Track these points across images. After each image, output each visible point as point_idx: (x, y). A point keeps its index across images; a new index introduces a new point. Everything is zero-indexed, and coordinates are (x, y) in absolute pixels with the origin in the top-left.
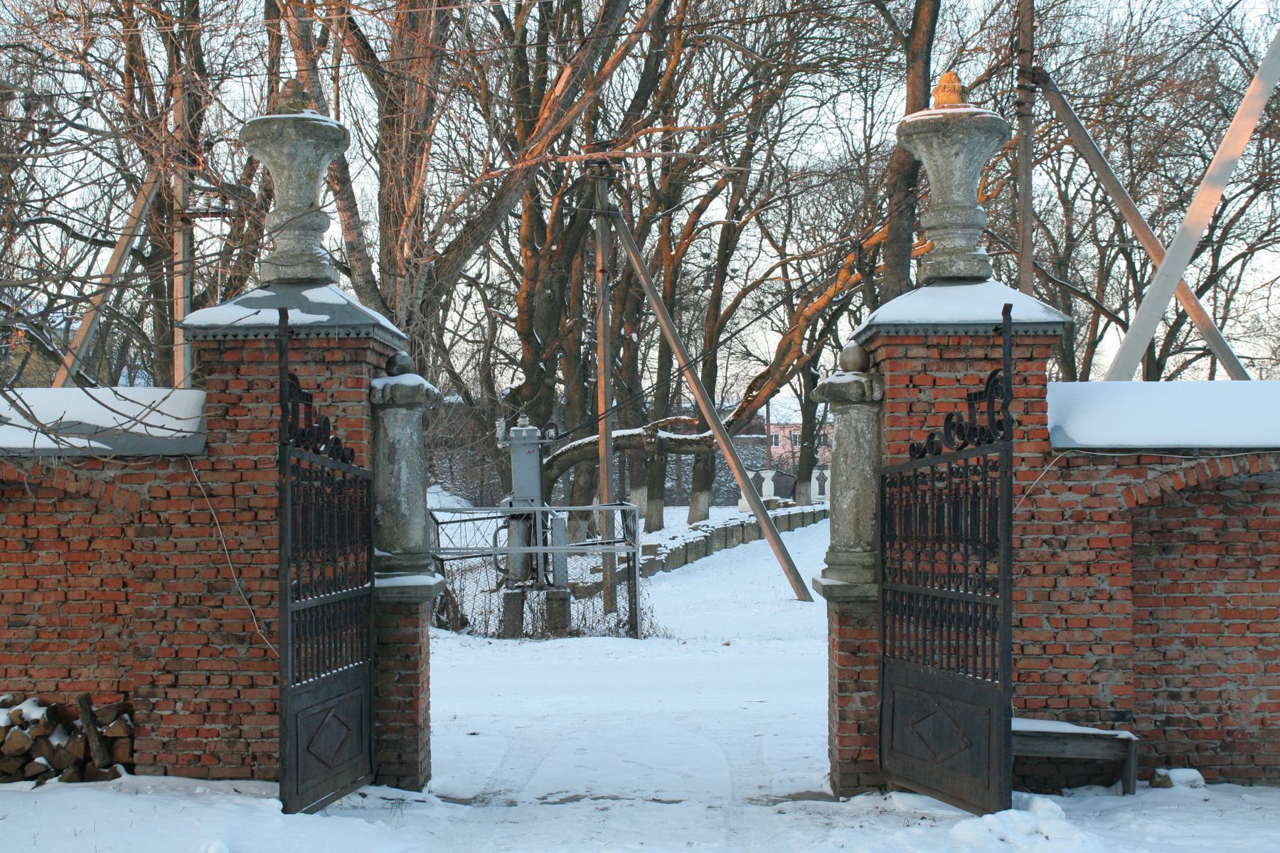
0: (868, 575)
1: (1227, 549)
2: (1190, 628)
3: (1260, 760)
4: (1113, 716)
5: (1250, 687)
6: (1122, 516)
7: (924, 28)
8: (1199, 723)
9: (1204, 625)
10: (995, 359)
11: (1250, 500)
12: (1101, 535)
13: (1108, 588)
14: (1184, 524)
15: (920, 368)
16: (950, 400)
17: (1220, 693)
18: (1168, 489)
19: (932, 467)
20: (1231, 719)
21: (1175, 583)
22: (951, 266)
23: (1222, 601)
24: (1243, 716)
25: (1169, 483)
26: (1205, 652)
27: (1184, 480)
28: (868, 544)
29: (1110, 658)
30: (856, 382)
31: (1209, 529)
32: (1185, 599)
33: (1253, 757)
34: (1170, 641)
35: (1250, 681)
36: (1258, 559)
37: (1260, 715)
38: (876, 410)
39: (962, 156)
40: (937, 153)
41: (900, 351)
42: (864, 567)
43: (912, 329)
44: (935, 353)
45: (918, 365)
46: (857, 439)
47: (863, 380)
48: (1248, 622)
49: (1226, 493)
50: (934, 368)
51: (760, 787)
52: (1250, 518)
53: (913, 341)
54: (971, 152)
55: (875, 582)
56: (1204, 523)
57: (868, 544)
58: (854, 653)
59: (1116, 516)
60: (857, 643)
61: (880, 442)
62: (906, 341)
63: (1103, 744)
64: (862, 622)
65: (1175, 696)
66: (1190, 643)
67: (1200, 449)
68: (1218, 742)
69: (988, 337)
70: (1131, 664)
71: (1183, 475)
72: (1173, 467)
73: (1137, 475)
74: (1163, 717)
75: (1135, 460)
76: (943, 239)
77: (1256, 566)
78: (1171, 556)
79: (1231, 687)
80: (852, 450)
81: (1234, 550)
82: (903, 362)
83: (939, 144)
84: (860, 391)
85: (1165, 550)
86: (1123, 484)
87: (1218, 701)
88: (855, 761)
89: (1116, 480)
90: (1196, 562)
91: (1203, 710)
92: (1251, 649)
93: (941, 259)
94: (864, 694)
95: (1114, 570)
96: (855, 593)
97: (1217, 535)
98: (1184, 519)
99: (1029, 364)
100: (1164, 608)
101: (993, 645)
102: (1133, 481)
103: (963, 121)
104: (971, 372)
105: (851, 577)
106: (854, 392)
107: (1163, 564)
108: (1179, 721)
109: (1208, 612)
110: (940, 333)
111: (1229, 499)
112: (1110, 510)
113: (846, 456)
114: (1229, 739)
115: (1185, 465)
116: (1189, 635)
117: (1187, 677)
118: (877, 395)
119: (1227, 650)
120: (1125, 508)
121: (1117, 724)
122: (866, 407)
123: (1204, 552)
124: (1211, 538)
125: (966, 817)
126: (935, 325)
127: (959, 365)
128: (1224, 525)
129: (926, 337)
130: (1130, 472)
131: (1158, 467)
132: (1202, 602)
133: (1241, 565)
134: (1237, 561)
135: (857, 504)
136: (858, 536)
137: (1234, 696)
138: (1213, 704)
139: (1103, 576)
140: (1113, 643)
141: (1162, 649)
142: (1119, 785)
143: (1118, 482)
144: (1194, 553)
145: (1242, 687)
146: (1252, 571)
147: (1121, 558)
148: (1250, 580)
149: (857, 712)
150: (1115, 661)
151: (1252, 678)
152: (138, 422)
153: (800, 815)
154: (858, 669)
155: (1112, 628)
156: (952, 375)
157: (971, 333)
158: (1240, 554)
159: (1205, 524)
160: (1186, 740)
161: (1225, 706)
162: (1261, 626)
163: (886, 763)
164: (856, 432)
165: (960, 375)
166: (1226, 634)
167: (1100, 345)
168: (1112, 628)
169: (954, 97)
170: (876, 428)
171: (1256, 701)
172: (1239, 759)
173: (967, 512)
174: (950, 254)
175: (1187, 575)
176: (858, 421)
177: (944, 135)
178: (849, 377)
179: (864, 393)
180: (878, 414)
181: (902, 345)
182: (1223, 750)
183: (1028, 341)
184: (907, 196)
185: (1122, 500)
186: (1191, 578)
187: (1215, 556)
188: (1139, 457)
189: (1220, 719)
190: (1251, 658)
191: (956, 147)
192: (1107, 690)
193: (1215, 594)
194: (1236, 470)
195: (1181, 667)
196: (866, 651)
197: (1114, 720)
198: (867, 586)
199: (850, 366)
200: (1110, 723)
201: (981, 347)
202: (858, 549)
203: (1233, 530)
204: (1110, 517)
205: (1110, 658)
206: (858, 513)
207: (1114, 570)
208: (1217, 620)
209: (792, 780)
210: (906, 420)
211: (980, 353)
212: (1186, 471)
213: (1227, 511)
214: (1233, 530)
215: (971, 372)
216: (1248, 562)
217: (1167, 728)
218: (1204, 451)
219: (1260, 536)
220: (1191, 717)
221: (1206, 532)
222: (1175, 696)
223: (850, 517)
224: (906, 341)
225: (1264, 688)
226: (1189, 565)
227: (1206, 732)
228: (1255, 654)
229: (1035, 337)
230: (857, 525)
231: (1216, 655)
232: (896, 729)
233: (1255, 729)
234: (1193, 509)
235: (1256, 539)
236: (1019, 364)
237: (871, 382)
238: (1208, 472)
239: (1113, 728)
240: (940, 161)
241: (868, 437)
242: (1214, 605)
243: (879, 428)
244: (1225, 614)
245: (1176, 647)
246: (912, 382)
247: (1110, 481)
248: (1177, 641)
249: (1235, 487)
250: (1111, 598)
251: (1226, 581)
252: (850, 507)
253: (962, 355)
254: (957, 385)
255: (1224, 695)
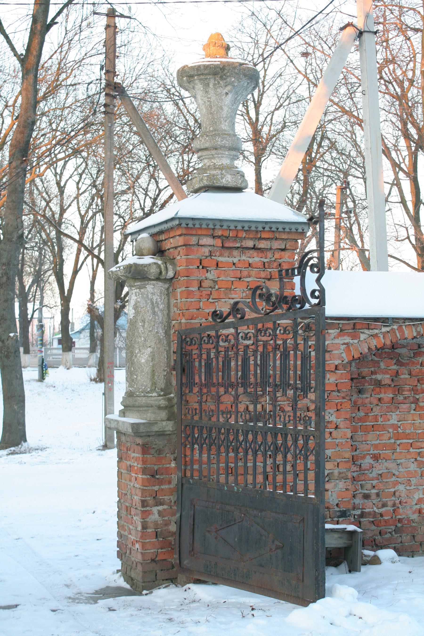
0: (164, 414)
1: (399, 390)
2: (376, 447)
3: (419, 538)
4: (338, 514)
5: (413, 487)
6: (344, 367)
7: (35, 53)
8: (381, 515)
9: (385, 445)
10: (260, 249)
11: (412, 355)
12: (331, 381)
13: (335, 420)
14: (372, 373)
15: (207, 254)
16: (229, 279)
17: (394, 493)
18: (373, 348)
19: (217, 332)
20: (401, 510)
21: (367, 415)
22: (222, 178)
23: (395, 427)
24: (408, 508)
25: (374, 343)
26: (386, 464)
27: (383, 341)
28: (162, 390)
29: (336, 472)
30: (155, 263)
31: (388, 376)
32: (373, 426)
33: (414, 536)
34: (364, 457)
35: (413, 483)
36: (417, 397)
37: (418, 507)
38: (166, 286)
39: (230, 96)
40: (211, 92)
41: (193, 240)
42: (160, 408)
43: (197, 223)
44: (218, 242)
45: (206, 251)
46: (153, 308)
47: (160, 262)
48: (411, 441)
49: (398, 351)
50: (218, 254)
51: (67, 586)
52: (412, 368)
53: (204, 232)
54: (237, 93)
55: (168, 419)
56: (385, 372)
57: (162, 390)
58: (153, 476)
59: (340, 367)
60: (156, 467)
61: (169, 311)
62: (199, 232)
63: (336, 535)
64: (159, 451)
65: (366, 497)
66: (376, 457)
67: (393, 318)
68: (393, 528)
69: (257, 232)
70: (349, 475)
71: (382, 337)
72: (376, 331)
73: (354, 337)
74: (358, 512)
75: (352, 326)
76: (214, 158)
77: (416, 401)
78: (365, 396)
79: (401, 487)
80: (149, 316)
81: (403, 391)
82: (195, 248)
83: (215, 85)
84: (158, 270)
85: (360, 392)
86: (344, 344)
87: (393, 498)
88: (153, 560)
89: (339, 341)
90: (380, 400)
91: (384, 505)
92: (413, 460)
93: (215, 172)
94: (160, 508)
95: (339, 407)
96: (155, 428)
97: (392, 380)
98: (373, 369)
99: (283, 253)
100: (359, 433)
101: (255, 465)
102: (351, 341)
103: (235, 68)
104: (243, 258)
105: (150, 416)
106: (154, 270)
107: (359, 402)
108: (369, 513)
109: (387, 436)
110: (225, 227)
111: (399, 355)
112: (337, 362)
113: (143, 321)
114: (399, 525)
115: (384, 330)
116: (376, 452)
117: (374, 482)
118: (171, 274)
119: (399, 461)
120: (346, 361)
121: (341, 519)
122: (160, 284)
123: (385, 393)
124: (388, 382)
125: (297, 608)
126: (221, 220)
127: (235, 253)
128: (397, 373)
129: (214, 229)
130: (349, 335)
131: (366, 331)
132: (383, 428)
133: (407, 401)
134: (405, 398)
135: (153, 359)
136: (154, 384)
137: (403, 495)
138: (390, 501)
139: (332, 411)
140: (339, 460)
141: (358, 463)
142: (344, 566)
143: (342, 342)
144: (378, 394)
145: (408, 488)
146: (413, 406)
147: (344, 398)
148: (412, 412)
149: (156, 523)
150: (340, 473)
151: (414, 481)
152: (182, 99)
153: (131, 611)
154: (156, 488)
155: (337, 449)
156: (230, 260)
157: (246, 228)
158: (406, 393)
159: (386, 373)
160: (374, 527)
161: (397, 502)
162: (419, 444)
163: (185, 562)
164: (152, 303)
165: (235, 260)
166: (398, 450)
167: (79, 273)
168: (337, 449)
169: (222, 51)
170: (166, 300)
171: (416, 496)
172: (406, 538)
173: (256, 365)
174: (221, 169)
175: (374, 409)
176: (153, 294)
177: (221, 78)
178: (148, 260)
179: (161, 273)
180: (168, 289)
181: (195, 235)
182: (396, 533)
183: (284, 236)
184: (22, 163)
185: (344, 355)
186: (376, 411)
187: (391, 396)
188: (354, 324)
189: (394, 511)
190: (413, 467)
191: (229, 88)
192: (335, 495)
193: (391, 422)
194: (415, 334)
195: (371, 475)
196: (162, 474)
197: (339, 517)
198: (164, 423)
199: (145, 252)
200: (336, 519)
201: (251, 239)
202: (155, 394)
203: (402, 376)
204: (336, 368)
205: (336, 472)
206: (153, 366)
207: (339, 407)
208: (392, 441)
209: (86, 577)
210: (197, 293)
211: (250, 244)
212: (384, 334)
213: (399, 363)
214: (402, 376)
215: (243, 258)
216: (411, 399)
217: (362, 520)
218: (395, 320)
219: (418, 381)
220: (377, 511)
221: (385, 378)
222: (366, 497)
223: (147, 369)
224: (199, 232)
225: (420, 488)
226: (375, 402)
227: (386, 521)
228: (416, 463)
229: (288, 233)
230: (153, 375)
231: (392, 465)
232: (197, 534)
233: (415, 517)
234: (378, 362)
235: (416, 383)
236: (276, 253)
237: (166, 263)
238: (398, 335)
239: (338, 523)
240: (213, 98)
241: (161, 307)
242: (391, 430)
243: (169, 300)
244: (398, 437)
245: (368, 460)
246: (202, 265)
247: (336, 341)
248: (368, 457)
249: (403, 346)
250: (337, 427)
251: (398, 413)
252: (147, 361)
253: (238, 245)
254: (234, 268)
255: (397, 494)
